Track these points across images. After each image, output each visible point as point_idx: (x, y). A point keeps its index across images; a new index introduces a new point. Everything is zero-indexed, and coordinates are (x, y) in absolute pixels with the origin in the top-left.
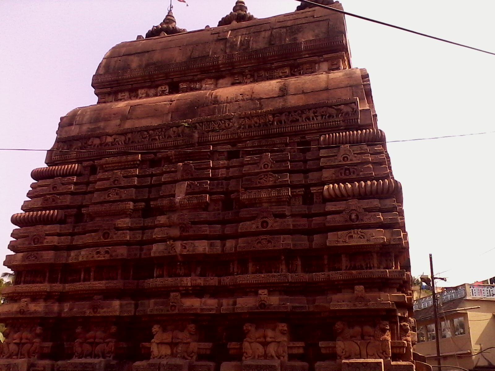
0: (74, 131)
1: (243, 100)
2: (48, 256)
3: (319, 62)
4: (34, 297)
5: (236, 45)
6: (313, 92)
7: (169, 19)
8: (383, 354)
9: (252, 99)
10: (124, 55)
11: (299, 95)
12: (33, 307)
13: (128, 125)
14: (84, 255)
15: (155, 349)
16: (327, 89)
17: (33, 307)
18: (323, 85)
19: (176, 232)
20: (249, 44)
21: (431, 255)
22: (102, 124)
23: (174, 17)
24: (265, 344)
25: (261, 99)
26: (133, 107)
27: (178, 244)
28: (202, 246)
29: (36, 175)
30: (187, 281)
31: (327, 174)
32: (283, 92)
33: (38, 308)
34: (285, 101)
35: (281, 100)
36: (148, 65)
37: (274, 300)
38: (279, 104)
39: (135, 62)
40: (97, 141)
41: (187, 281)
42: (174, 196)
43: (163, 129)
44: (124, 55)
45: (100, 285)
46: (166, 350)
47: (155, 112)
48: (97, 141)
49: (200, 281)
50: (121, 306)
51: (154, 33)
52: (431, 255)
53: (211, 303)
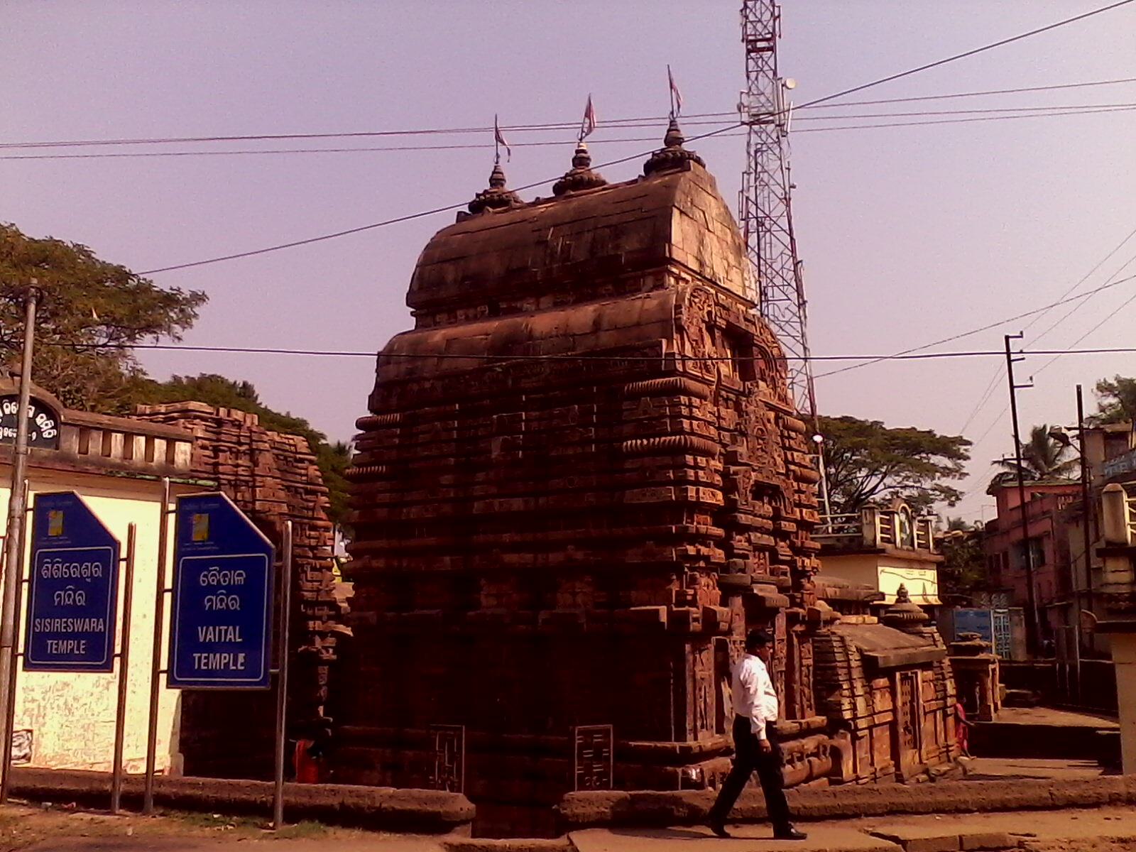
0: (392, 370)
1: (557, 336)
2: (382, 513)
3: (644, 276)
4: (375, 553)
5: (556, 253)
6: (627, 328)
7: (497, 180)
8: (667, 602)
9: (565, 335)
10: (438, 262)
11: (611, 332)
12: (375, 564)
13: (445, 365)
14: (414, 512)
15: (484, 601)
16: (638, 324)
17: (375, 564)
18: (635, 318)
19: (494, 490)
20: (569, 251)
21: (1079, 388)
22: (419, 363)
23: (502, 173)
24: (574, 594)
25: (575, 335)
26: (450, 341)
27: (496, 502)
28: (517, 504)
29: (360, 424)
30: (506, 537)
31: (627, 429)
32: (597, 325)
33: (379, 564)
34: (598, 338)
35: (593, 337)
36: (465, 278)
37: (579, 555)
38: (591, 341)
39: (451, 273)
40: (415, 387)
41: (506, 537)
42: (490, 452)
43: (478, 373)
44: (438, 262)
45: (431, 541)
46: (493, 602)
47: (469, 349)
48: (415, 387)
49: (517, 538)
50: (451, 560)
51: (477, 206)
52: (1079, 388)
53: (529, 557)
